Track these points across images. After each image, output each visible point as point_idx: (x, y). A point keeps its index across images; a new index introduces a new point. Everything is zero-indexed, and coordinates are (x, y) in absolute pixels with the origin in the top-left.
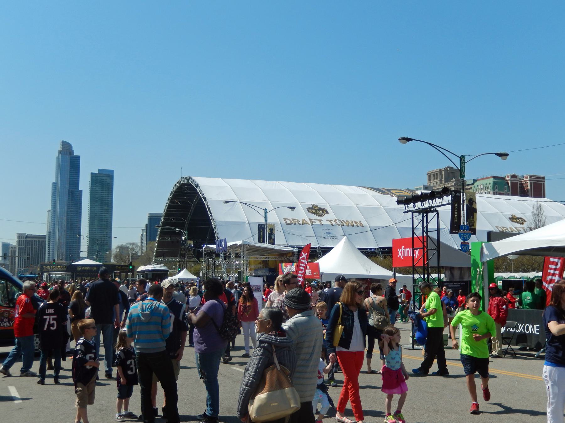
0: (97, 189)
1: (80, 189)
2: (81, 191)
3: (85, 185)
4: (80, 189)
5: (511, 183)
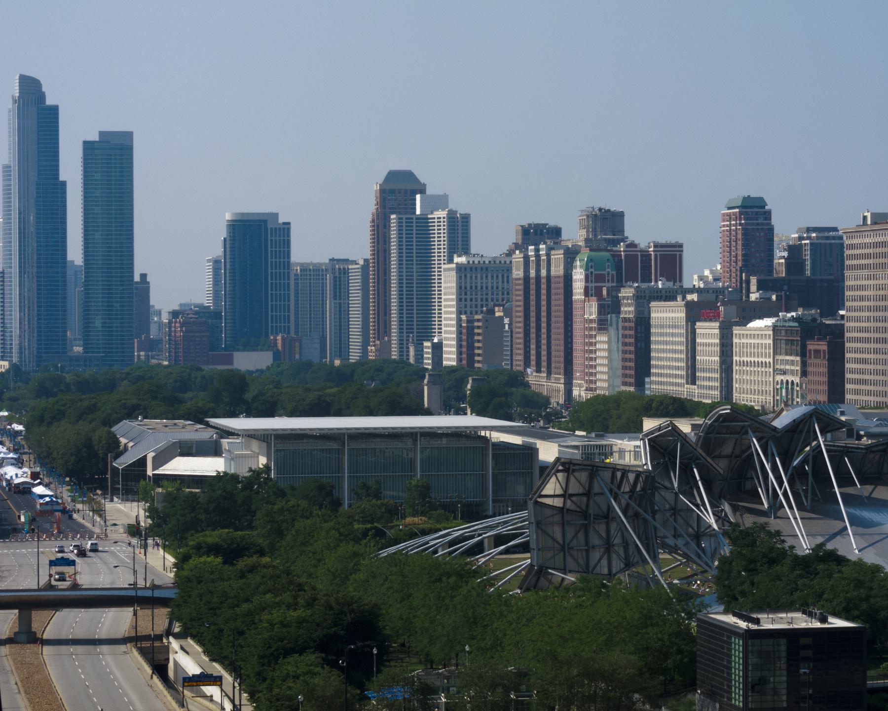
0: (97, 176)
1: (61, 179)
2: (101, 134)
3: (71, 169)
4: (61, 179)
5: (626, 255)
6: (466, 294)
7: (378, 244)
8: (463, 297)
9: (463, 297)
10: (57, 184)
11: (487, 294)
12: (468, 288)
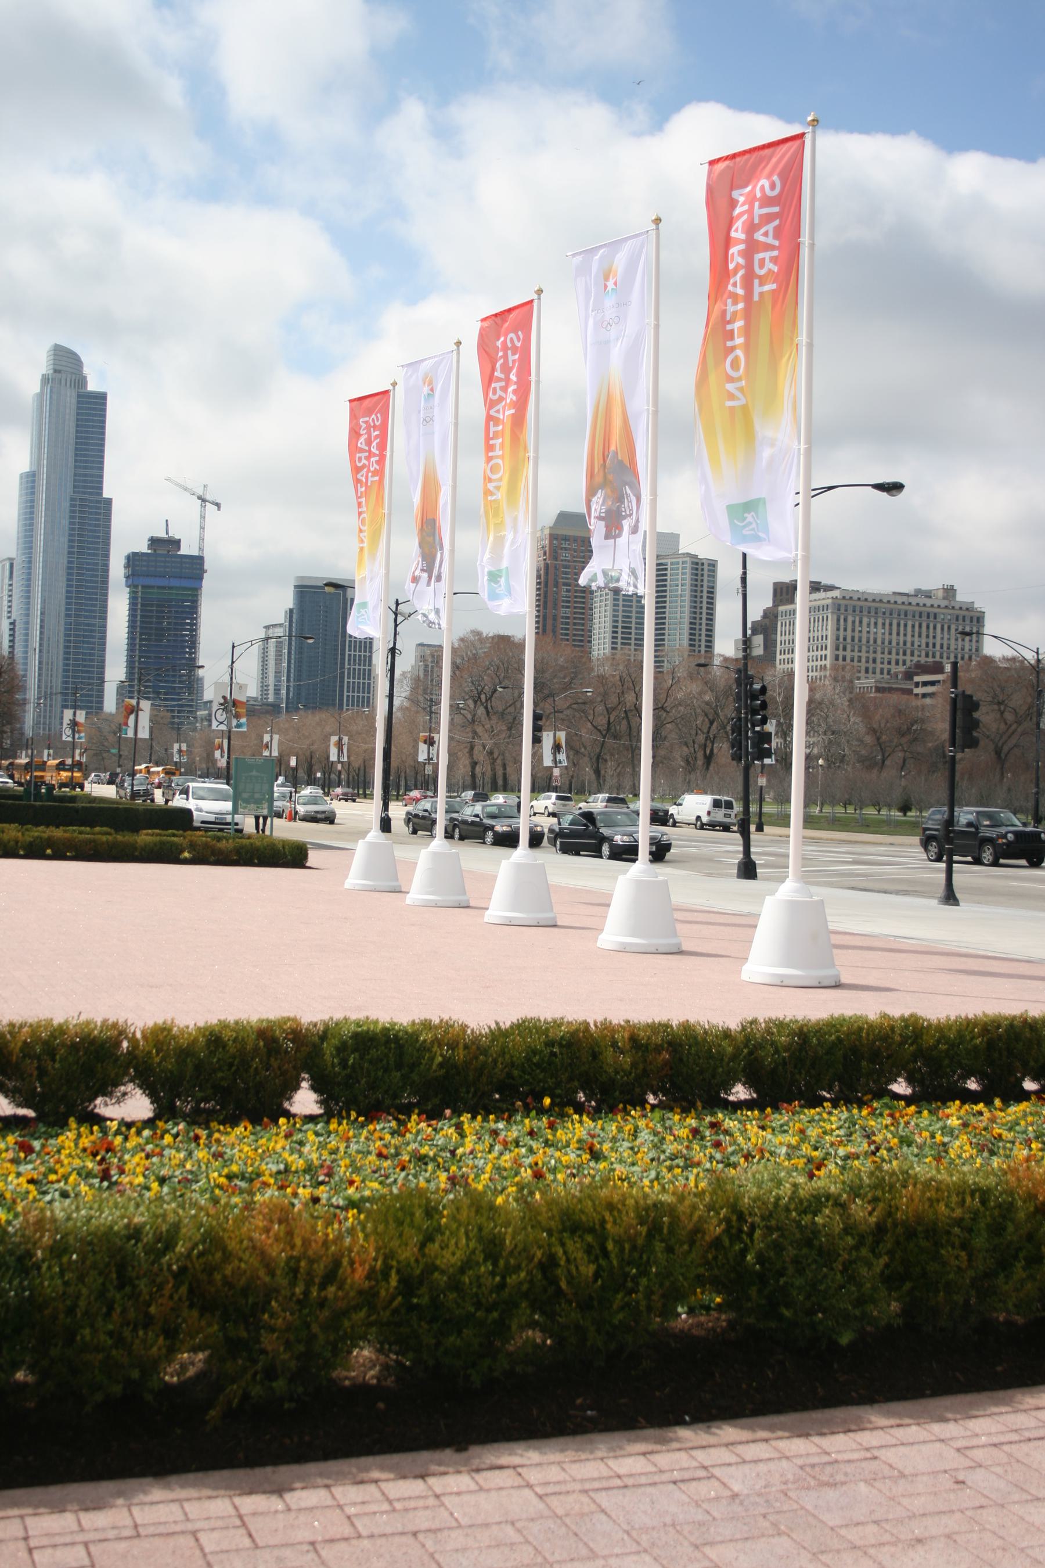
1: (105, 495)
2: (109, 501)
4: (105, 495)
6: (845, 649)
7: (545, 608)
8: (841, 653)
9: (841, 653)
10: (99, 502)
11: (875, 652)
12: (849, 640)
